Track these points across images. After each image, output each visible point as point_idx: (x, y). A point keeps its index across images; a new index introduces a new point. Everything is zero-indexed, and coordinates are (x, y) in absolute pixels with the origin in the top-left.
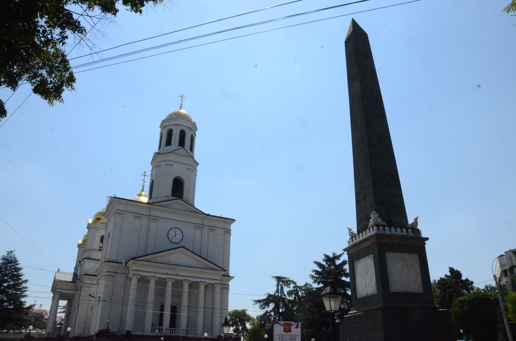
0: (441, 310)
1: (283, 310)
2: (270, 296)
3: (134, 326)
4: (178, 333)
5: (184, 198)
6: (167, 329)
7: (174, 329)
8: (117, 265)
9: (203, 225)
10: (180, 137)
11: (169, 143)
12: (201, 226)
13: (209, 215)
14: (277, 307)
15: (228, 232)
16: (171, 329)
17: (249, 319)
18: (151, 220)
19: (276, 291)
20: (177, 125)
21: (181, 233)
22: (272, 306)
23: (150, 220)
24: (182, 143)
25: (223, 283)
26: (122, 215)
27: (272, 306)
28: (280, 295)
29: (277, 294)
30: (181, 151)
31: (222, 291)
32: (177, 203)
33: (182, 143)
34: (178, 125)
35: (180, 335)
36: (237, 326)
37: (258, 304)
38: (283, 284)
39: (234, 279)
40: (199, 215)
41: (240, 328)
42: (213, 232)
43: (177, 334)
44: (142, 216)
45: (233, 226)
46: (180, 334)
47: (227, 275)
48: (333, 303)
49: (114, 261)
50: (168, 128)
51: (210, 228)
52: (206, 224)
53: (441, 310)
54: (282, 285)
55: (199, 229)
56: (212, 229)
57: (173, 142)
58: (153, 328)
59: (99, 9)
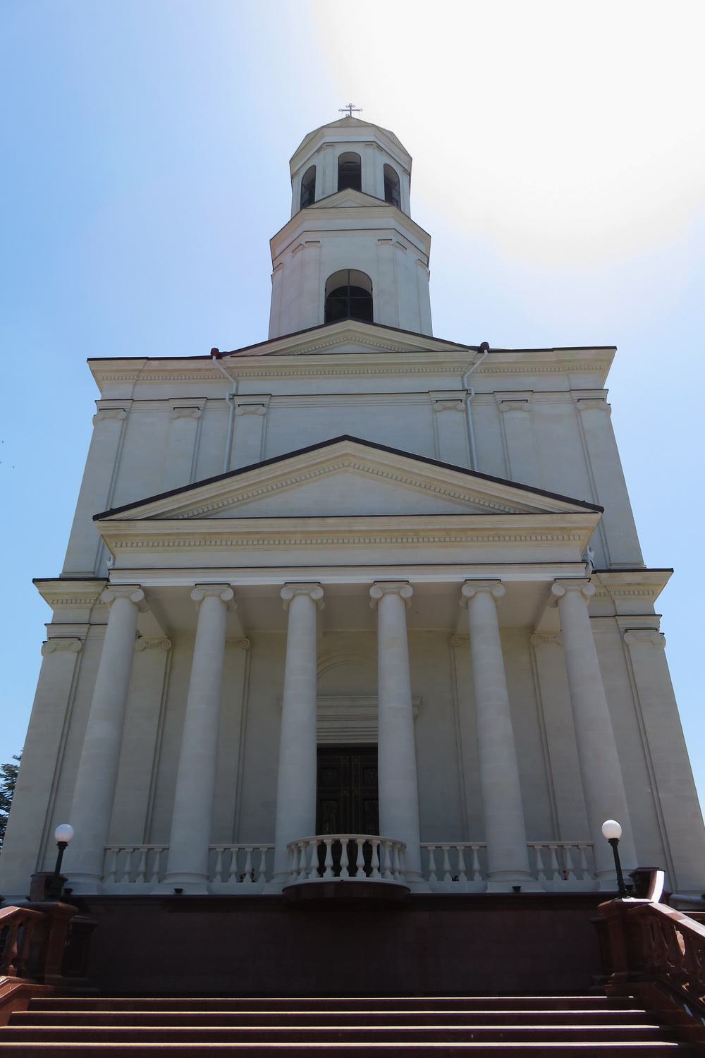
0: (632, 900)
3: (530, 847)
4: (356, 869)
6: (295, 848)
7: (361, 839)
8: (91, 587)
9: (468, 392)
12: (462, 396)
15: (597, 397)
16: (328, 839)
23: (234, 408)
25: (623, 607)
31: (625, 646)
39: (673, 579)
40: (442, 357)
42: (521, 409)
43: (337, 874)
44: (201, 403)
45: (616, 383)
46: (383, 875)
47: (619, 556)
51: (500, 397)
52: (480, 390)
53: (632, 900)
56: (511, 399)
58: (460, 848)
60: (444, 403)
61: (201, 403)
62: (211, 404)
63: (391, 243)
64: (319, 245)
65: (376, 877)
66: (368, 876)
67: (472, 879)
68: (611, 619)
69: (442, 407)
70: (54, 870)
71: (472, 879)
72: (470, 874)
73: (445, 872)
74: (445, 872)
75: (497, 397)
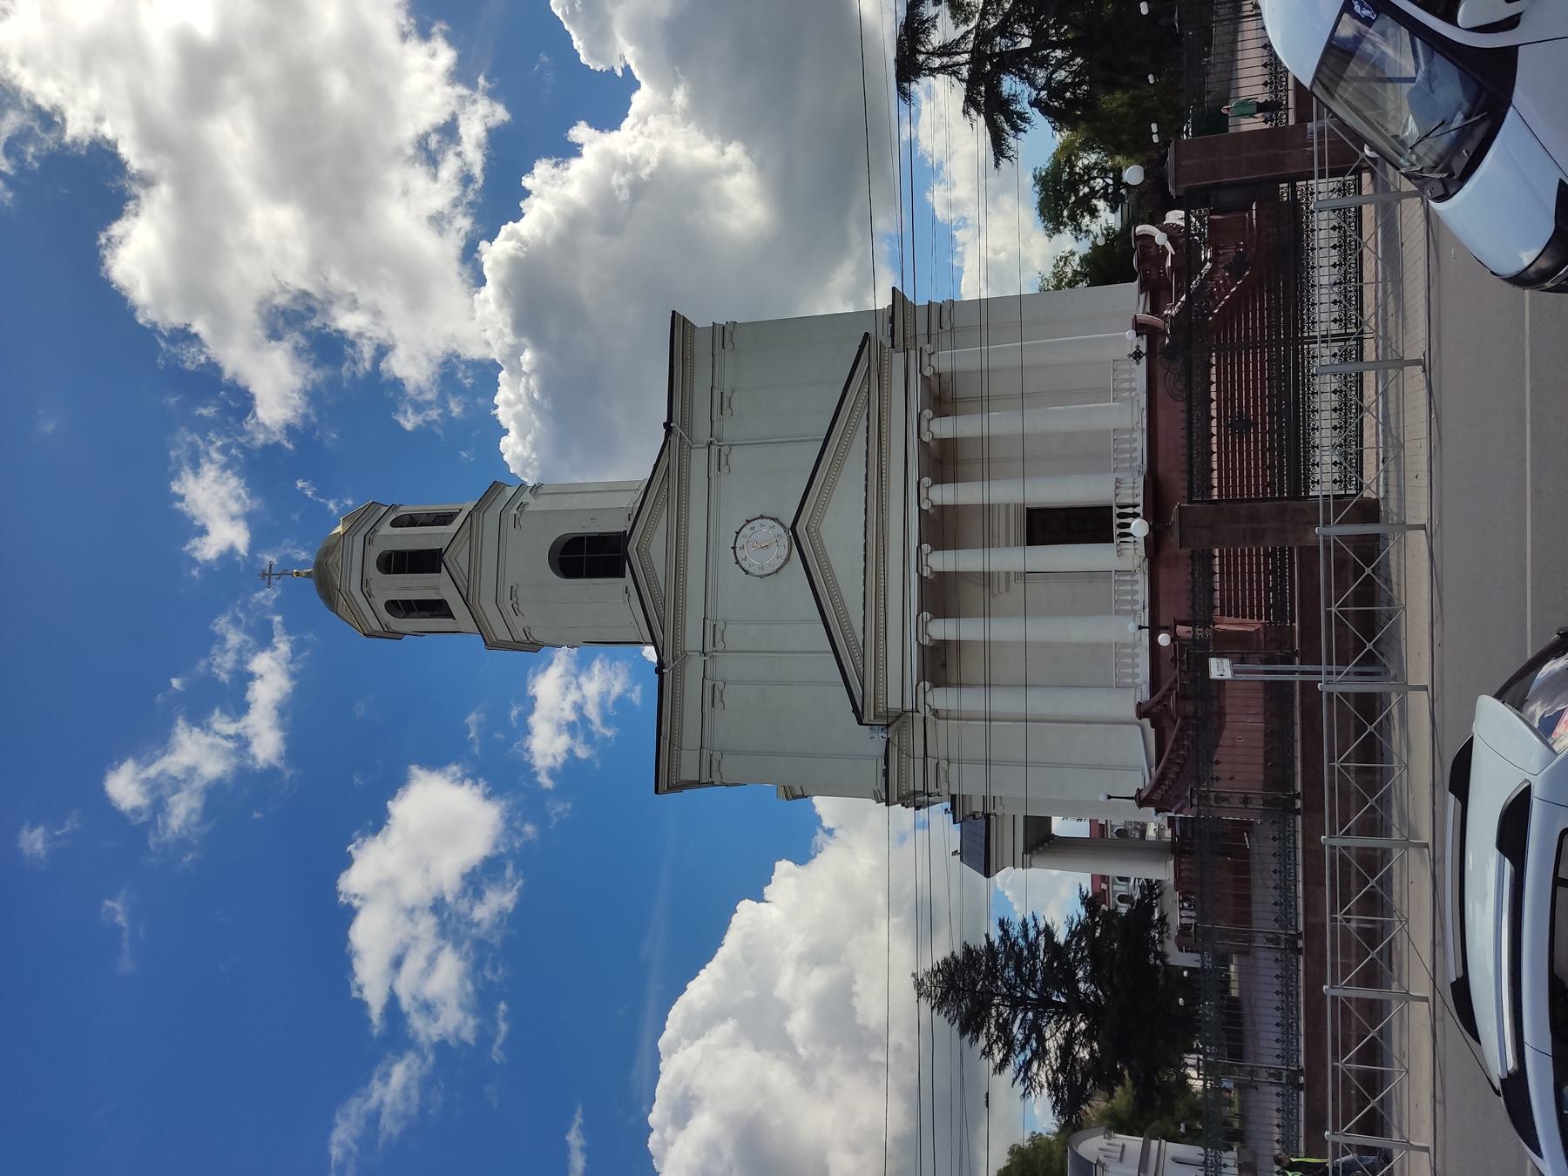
1: (1026, 31)
2: (970, 101)
4: (1135, 513)
5: (625, 529)
10: (410, 572)
11: (437, 608)
12: (714, 449)
13: (667, 426)
14: (1013, 62)
16: (1117, 531)
17: (1066, 155)
18: (720, 646)
19: (955, 73)
20: (365, 590)
21: (751, 525)
22: (1009, 85)
24: (427, 561)
26: (717, 756)
27: (1009, 85)
28: (966, 56)
29: (965, 72)
30: (459, 558)
32: (654, 549)
33: (427, 561)
34: (364, 582)
35: (1142, 505)
36: (1093, 193)
37: (1012, 141)
38: (923, 49)
41: (1098, 183)
44: (708, 683)
48: (1248, 63)
49: (885, 767)
50: (387, 617)
54: (927, 53)
55: (727, 456)
57: (433, 596)
59: (968, 4)
60: (726, 341)
61: (708, 683)
62: (705, 745)
63: (518, 515)
64: (515, 587)
65: (1140, 500)
66: (1139, 505)
67: (1137, 581)
68: (927, 696)
69: (728, 409)
70: (1161, 625)
71: (1137, 581)
72: (1131, 380)
73: (1131, 447)
74: (1131, 447)
75: (708, 651)
